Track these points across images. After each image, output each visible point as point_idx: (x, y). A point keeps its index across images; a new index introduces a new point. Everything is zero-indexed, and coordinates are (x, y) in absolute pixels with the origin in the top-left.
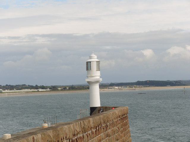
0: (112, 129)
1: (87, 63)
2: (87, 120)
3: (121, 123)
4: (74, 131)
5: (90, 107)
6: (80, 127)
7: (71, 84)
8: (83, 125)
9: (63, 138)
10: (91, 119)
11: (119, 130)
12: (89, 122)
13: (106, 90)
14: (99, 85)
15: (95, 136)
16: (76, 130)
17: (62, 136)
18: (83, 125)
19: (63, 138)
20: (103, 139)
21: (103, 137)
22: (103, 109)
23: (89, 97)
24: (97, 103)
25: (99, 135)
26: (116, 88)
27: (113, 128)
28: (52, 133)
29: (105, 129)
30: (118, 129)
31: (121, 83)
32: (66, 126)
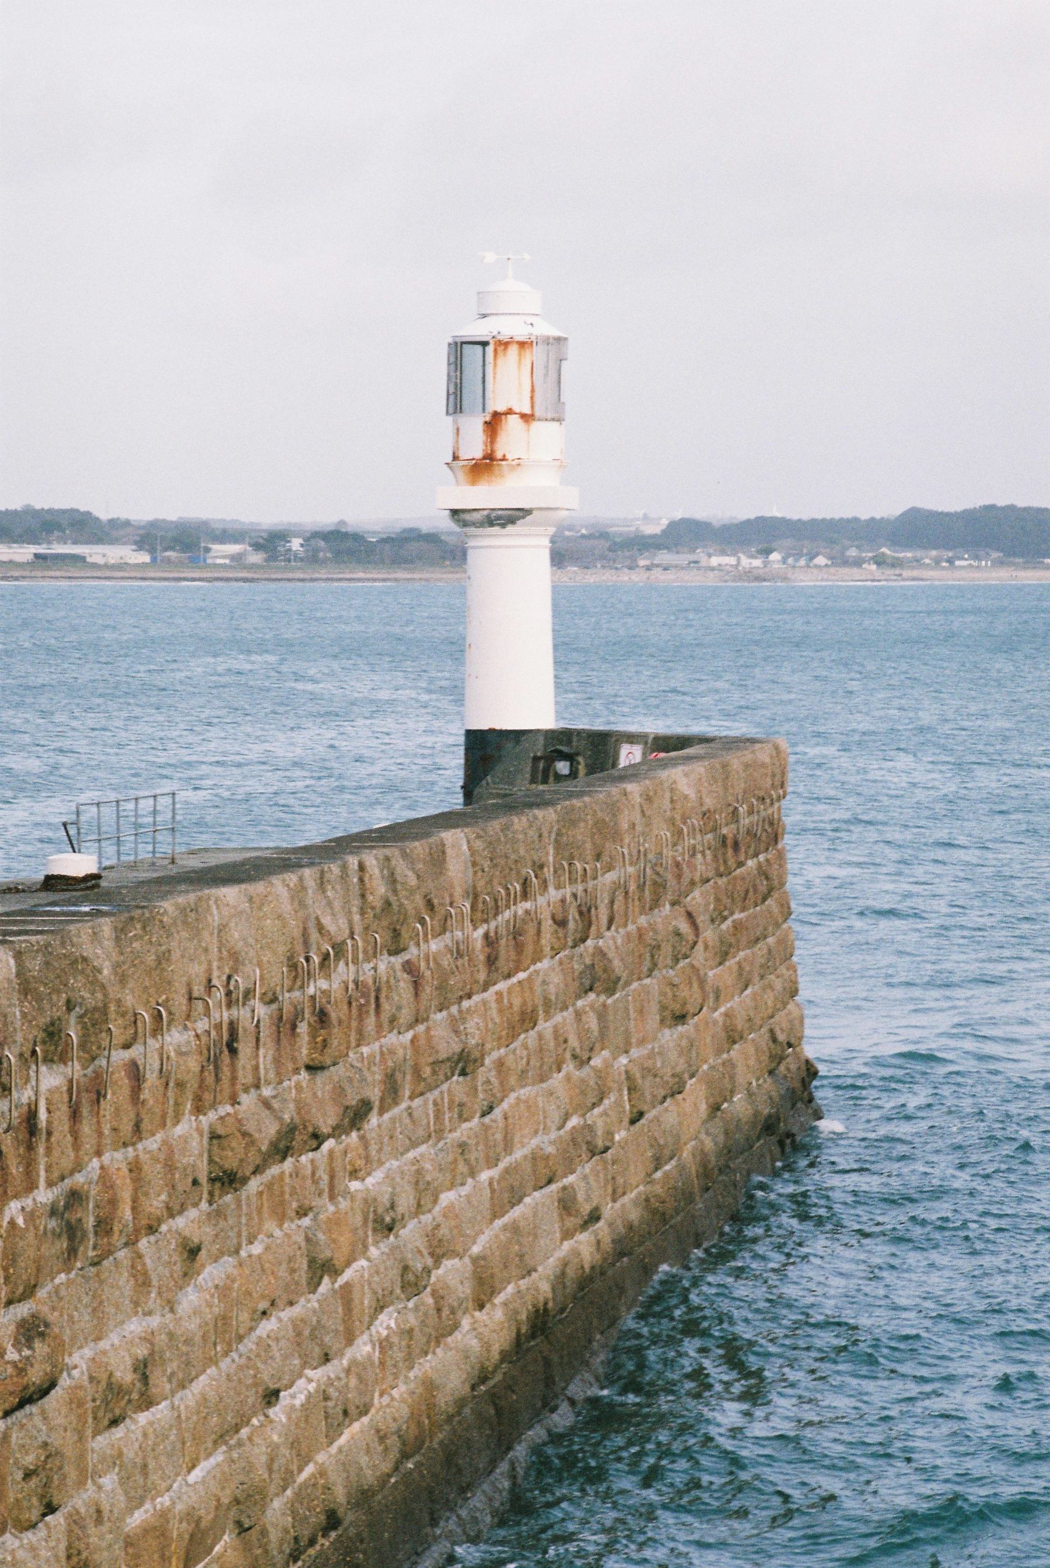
0: (631, 927)
1: (458, 348)
2: (418, 847)
3: (722, 882)
4: (297, 933)
5: (469, 733)
6: (356, 902)
7: (325, 518)
8: (379, 889)
9: (198, 990)
10: (456, 841)
11: (697, 935)
12: (438, 859)
13: (597, 577)
14: (546, 542)
15: (482, 976)
16: (320, 928)
17: (197, 970)
18: (379, 889)
19: (198, 990)
20: (547, 1004)
21: (552, 989)
22: (577, 755)
23: (448, 650)
24: (524, 697)
25: (522, 975)
26: (715, 561)
27: (643, 920)
28: (109, 944)
29: (571, 925)
30: (684, 927)
31: (813, 521)
32: (230, 894)
